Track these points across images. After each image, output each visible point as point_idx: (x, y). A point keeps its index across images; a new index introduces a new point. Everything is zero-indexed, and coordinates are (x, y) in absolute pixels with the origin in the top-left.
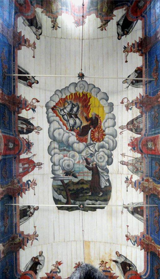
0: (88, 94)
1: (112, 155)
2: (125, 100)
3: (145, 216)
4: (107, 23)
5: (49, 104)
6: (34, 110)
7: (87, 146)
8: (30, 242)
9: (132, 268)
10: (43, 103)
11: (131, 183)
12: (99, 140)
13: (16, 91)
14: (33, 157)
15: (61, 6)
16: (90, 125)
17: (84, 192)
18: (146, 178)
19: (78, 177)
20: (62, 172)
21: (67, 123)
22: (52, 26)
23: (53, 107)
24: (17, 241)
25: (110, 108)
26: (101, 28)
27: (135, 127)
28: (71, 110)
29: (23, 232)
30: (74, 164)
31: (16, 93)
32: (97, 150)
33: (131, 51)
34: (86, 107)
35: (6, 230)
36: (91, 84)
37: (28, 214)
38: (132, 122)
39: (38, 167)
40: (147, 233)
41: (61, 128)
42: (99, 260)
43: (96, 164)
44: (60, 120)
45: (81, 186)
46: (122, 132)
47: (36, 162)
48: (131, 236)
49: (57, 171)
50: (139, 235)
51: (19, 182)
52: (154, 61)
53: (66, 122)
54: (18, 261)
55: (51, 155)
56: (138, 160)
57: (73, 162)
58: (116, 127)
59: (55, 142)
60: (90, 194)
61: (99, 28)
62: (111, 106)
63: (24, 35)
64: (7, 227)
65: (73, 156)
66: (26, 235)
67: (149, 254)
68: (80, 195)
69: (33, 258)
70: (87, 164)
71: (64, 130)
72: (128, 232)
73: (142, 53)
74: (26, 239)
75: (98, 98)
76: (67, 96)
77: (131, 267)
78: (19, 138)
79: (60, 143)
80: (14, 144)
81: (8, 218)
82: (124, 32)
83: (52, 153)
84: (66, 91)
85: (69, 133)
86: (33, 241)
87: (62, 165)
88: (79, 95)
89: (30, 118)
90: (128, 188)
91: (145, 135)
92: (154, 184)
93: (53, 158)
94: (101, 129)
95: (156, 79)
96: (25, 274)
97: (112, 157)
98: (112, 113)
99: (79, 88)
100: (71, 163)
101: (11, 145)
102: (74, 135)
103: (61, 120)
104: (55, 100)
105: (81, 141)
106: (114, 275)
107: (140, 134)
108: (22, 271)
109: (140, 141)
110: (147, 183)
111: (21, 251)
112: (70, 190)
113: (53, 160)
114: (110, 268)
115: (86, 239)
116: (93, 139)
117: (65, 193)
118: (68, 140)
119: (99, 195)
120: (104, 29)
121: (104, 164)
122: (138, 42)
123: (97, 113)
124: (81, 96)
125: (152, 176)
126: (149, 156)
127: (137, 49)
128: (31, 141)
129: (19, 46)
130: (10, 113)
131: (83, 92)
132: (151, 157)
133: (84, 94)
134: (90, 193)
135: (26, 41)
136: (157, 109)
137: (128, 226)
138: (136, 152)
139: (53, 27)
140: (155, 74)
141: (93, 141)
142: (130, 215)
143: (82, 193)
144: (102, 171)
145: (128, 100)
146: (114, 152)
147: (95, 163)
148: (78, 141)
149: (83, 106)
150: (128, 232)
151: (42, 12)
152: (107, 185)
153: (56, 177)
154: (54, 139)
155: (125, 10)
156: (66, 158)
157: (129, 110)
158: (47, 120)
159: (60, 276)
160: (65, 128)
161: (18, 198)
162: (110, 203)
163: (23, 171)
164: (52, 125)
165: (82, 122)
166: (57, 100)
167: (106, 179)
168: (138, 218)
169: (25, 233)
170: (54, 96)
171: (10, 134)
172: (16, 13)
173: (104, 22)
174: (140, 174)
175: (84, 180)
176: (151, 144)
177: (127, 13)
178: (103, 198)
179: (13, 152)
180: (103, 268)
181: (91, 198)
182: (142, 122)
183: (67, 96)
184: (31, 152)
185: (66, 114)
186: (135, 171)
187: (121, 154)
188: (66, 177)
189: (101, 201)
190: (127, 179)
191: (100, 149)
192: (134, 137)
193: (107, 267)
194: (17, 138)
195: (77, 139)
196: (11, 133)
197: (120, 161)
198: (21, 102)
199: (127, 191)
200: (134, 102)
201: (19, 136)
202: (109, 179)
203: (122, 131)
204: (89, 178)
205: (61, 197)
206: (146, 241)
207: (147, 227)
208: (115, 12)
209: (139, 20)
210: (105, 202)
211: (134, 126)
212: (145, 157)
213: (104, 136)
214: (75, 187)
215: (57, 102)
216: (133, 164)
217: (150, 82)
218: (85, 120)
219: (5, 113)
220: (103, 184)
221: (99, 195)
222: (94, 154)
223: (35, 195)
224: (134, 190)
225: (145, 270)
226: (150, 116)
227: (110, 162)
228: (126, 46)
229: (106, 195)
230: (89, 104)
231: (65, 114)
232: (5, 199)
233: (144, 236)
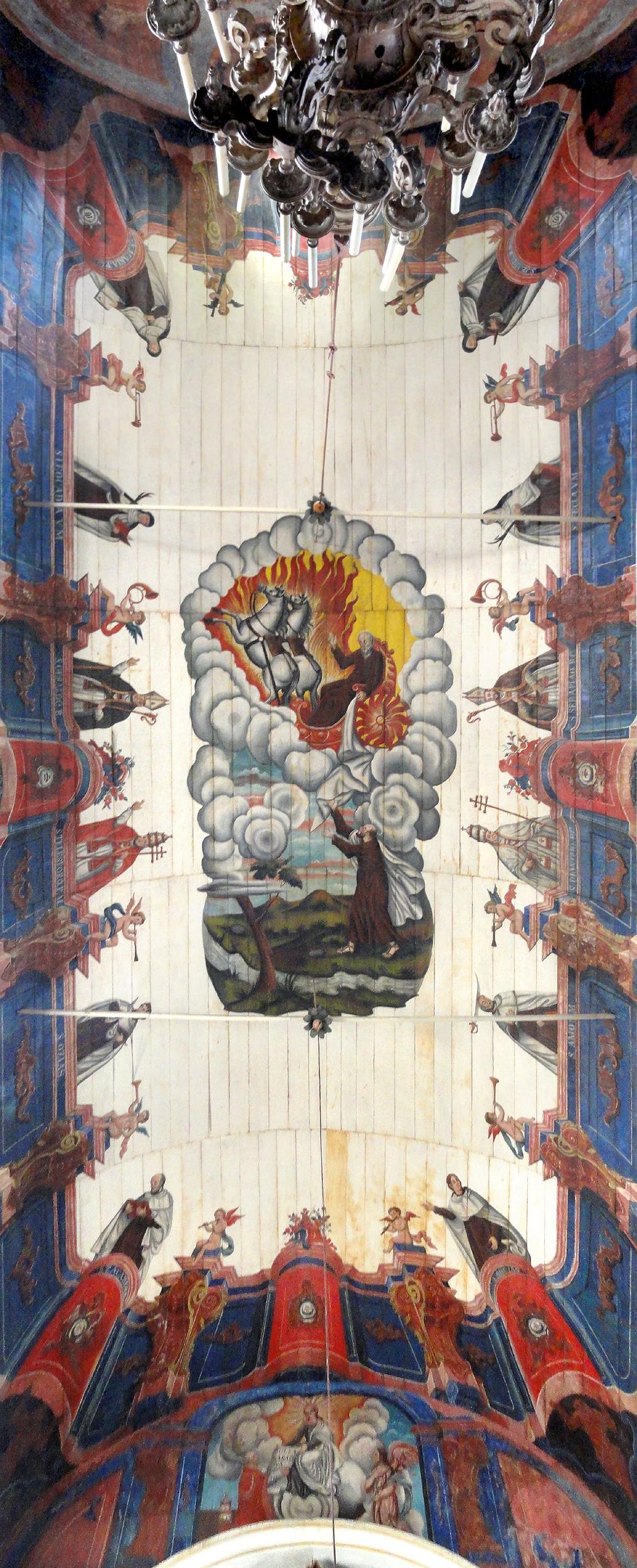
0: (344, 561)
1: (435, 799)
2: (491, 591)
3: (562, 1050)
4: (423, 285)
5: (195, 603)
6: (135, 631)
7: (340, 763)
8: (116, 1144)
9: (510, 1244)
10: (170, 601)
11: (510, 913)
12: (385, 741)
13: (65, 562)
14: (131, 814)
15: (246, 225)
16: (351, 681)
17: (326, 940)
18: (570, 902)
19: (304, 881)
20: (243, 863)
21: (264, 674)
22: (210, 301)
23: (208, 615)
24: (67, 1144)
25: (431, 618)
26: (397, 307)
27: (530, 698)
28: (281, 621)
29: (88, 1109)
30: (288, 832)
31: (66, 570)
32: (377, 776)
33: (516, 398)
34: (340, 613)
35: (24, 1114)
36: (358, 521)
37: (109, 1036)
38: (515, 678)
39: (148, 849)
40: (572, 1117)
41: (242, 695)
42: (382, 1204)
43: (373, 834)
44: (236, 662)
45: (314, 918)
46: (476, 713)
47: (142, 830)
48: (506, 1119)
49: (223, 859)
50: (540, 1119)
51: (74, 917)
52: (609, 447)
53: (258, 670)
54: (67, 1224)
55: (200, 801)
56: (538, 827)
57: (284, 825)
58: (454, 694)
59: (217, 750)
60: (350, 948)
61: (389, 304)
62: (436, 607)
63: (99, 345)
64: (26, 1102)
65: (287, 802)
66: (101, 1119)
67: (577, 1198)
68: (312, 953)
69: (129, 1206)
70: (338, 831)
71: (250, 701)
72: (495, 1104)
73: (558, 410)
74: (101, 1134)
75: (384, 574)
76: (263, 570)
77: (504, 1241)
78: (78, 745)
79: (237, 751)
80: (59, 774)
81: (30, 1062)
82: (487, 325)
83: (206, 792)
84: (261, 550)
85: (269, 712)
86: (127, 1138)
87: (244, 835)
88: (313, 564)
89: (121, 664)
90: (497, 932)
91: (567, 733)
92: (602, 929)
93: (208, 812)
94: (393, 699)
95: (615, 518)
96: (96, 1266)
97: (437, 807)
98: (437, 635)
99: (310, 537)
100: (278, 830)
101: (46, 778)
102: (290, 721)
103: (240, 664)
104: (216, 587)
105: (314, 742)
106: (440, 1265)
107: (548, 728)
108: (86, 1260)
109: (547, 755)
110: (573, 920)
111: (83, 1184)
112: (272, 934)
113: (208, 822)
114: (422, 1234)
115: (332, 1119)
116: (364, 737)
117: (253, 948)
118: (268, 742)
119: (385, 954)
120: (409, 308)
121: (404, 832)
122: (543, 367)
123: (380, 635)
124: (319, 567)
125: (591, 898)
126: (580, 816)
127: (540, 390)
128: (125, 754)
129: (81, 384)
130: (41, 649)
131: (324, 555)
132: (592, 824)
133: (331, 559)
134: (351, 944)
135: (106, 365)
136: (619, 639)
137: (495, 1081)
138: (530, 797)
139: (214, 305)
140: (613, 499)
141: (363, 744)
142: (504, 1040)
143: (318, 943)
144: (397, 862)
145: (501, 590)
146: (445, 791)
147: (369, 827)
148: (303, 744)
149: (323, 608)
150: (495, 1104)
151: (171, 251)
152: (415, 915)
153: (222, 885)
154: (211, 737)
155: (493, 238)
156: (257, 810)
157: (505, 630)
158: (185, 664)
159: (233, 1267)
160: (256, 695)
161: (71, 978)
162: (426, 985)
163: (90, 870)
164: (205, 683)
165: (322, 669)
166: (226, 584)
167: (412, 891)
168: (535, 1054)
169: (99, 1112)
170: (216, 569)
171: (41, 734)
172: (69, 263)
173: (410, 282)
174: (545, 881)
175: (325, 892)
176: (589, 772)
177: (502, 251)
178: (397, 967)
179: (54, 801)
180: (396, 1234)
181: (352, 965)
182: (556, 682)
183: (263, 570)
184: (122, 797)
185: (261, 639)
186: (525, 869)
187: (471, 800)
188: (260, 882)
189: (391, 976)
190: (494, 896)
191: (389, 774)
192: (524, 737)
193: (414, 1231)
194: (70, 744)
195: (302, 737)
196: (47, 729)
197: (466, 826)
198: (86, 603)
199: (494, 944)
200: (525, 601)
201: (76, 735)
202: (423, 892)
203: (474, 708)
204: (345, 887)
205: (237, 963)
206: (567, 1148)
207: (572, 1092)
208: (454, 246)
209: (546, 281)
210: (409, 982)
211: (523, 691)
212: (567, 818)
213: (405, 727)
214: (292, 924)
215: (225, 594)
216: (517, 841)
217: (589, 527)
218: (333, 661)
219: (24, 656)
220: (402, 912)
221: (385, 954)
222: (369, 793)
223: (136, 959)
224: (520, 942)
225: (558, 1257)
226: (588, 662)
227: (427, 829)
228: (497, 378)
229: (413, 953)
230: (349, 600)
231: (255, 638)
232: (19, 990)
233: (557, 1128)
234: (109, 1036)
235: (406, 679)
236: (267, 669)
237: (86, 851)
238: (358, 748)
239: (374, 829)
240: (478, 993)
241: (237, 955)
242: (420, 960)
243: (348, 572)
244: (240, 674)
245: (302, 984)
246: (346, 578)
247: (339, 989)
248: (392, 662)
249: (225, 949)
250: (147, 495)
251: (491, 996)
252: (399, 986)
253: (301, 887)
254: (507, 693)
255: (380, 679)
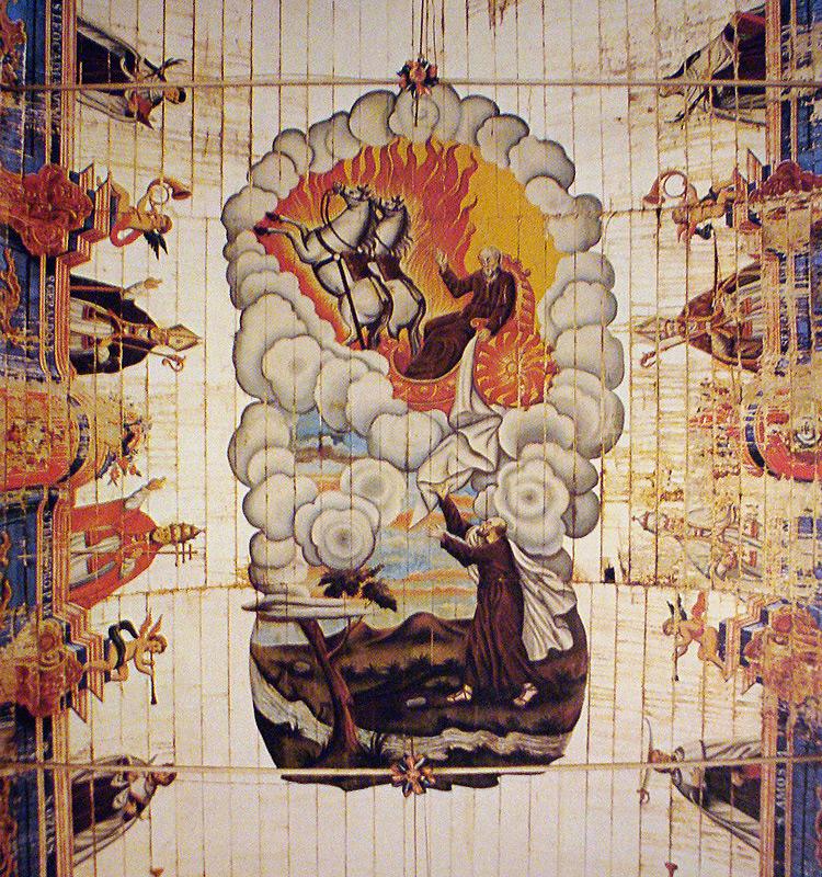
0: (456, 152)
1: (598, 478)
2: (674, 186)
6: (156, 241)
16: (468, 313)
17: (430, 684)
19: (399, 601)
21: (340, 303)
27: (728, 329)
28: (366, 234)
32: (509, 449)
38: (701, 306)
43: (501, 531)
55: (247, 483)
58: (619, 329)
60: (466, 694)
89: (135, 286)
94: (531, 337)
98: (592, 249)
102: (380, 372)
103: (305, 290)
112: (350, 675)
116: (487, 393)
119: (516, 701)
133: (437, 149)
134: (467, 688)
144: (538, 570)
147: (495, 522)
149: (425, 215)
156: (330, 497)
157: (696, 239)
161: (63, 719)
164: (254, 315)
185: (337, 257)
189: (525, 731)
195: (396, 393)
205: (297, 715)
214: (382, 661)
215: (284, 195)
221: (516, 701)
234: (116, 805)
235: (549, 311)
236: (346, 298)
237: (83, 544)
238: (480, 408)
239: (504, 524)
240: (650, 748)
241: (300, 703)
242: (570, 711)
243: (463, 164)
244: (306, 305)
245: (395, 745)
246: (460, 174)
247: (448, 751)
248: (529, 288)
249: (281, 692)
250: (176, 63)
251: (666, 748)
252: (533, 744)
253: (395, 609)
254: (699, 323)
255: (509, 311)
